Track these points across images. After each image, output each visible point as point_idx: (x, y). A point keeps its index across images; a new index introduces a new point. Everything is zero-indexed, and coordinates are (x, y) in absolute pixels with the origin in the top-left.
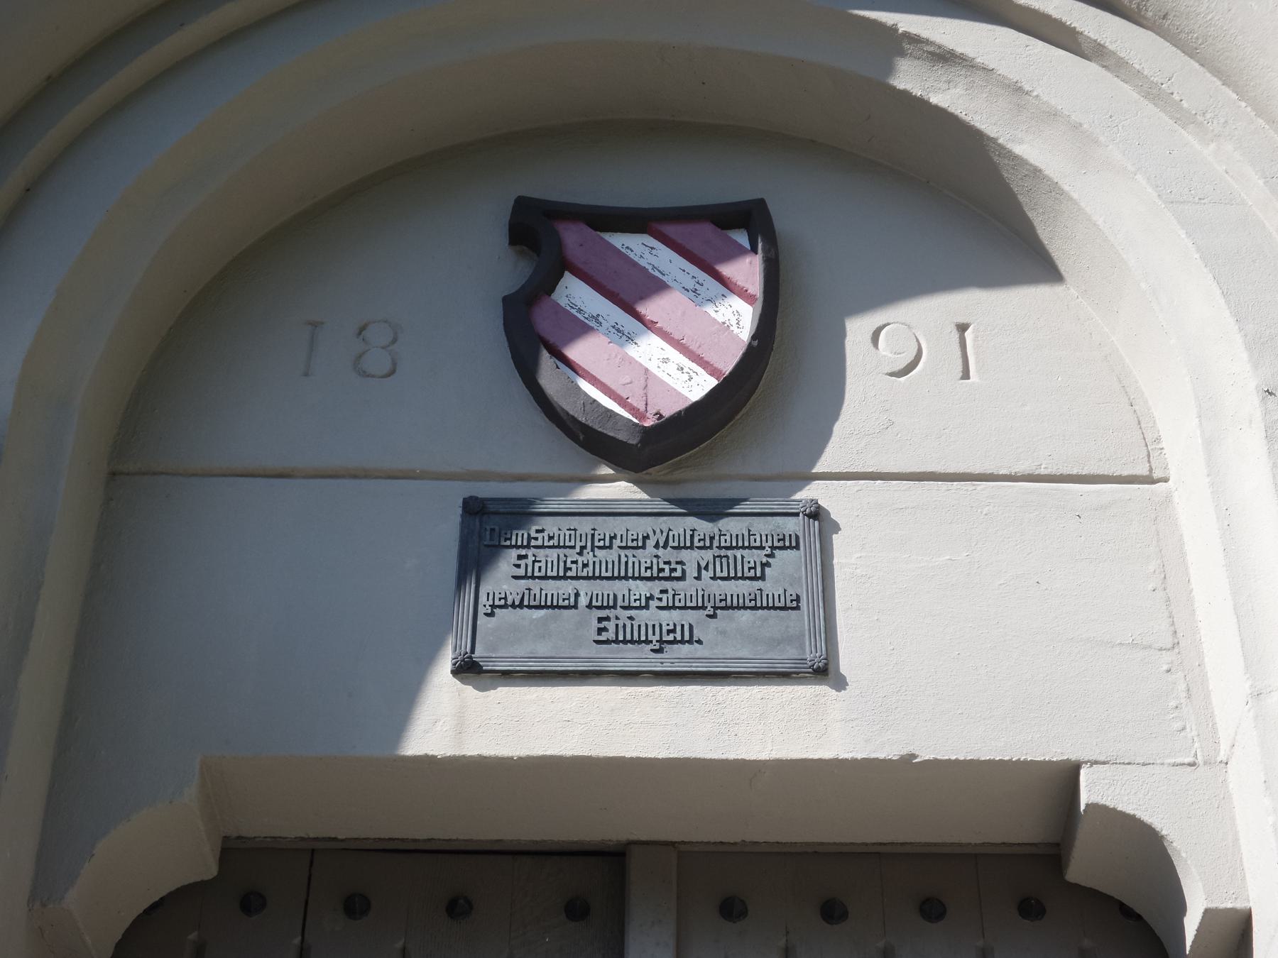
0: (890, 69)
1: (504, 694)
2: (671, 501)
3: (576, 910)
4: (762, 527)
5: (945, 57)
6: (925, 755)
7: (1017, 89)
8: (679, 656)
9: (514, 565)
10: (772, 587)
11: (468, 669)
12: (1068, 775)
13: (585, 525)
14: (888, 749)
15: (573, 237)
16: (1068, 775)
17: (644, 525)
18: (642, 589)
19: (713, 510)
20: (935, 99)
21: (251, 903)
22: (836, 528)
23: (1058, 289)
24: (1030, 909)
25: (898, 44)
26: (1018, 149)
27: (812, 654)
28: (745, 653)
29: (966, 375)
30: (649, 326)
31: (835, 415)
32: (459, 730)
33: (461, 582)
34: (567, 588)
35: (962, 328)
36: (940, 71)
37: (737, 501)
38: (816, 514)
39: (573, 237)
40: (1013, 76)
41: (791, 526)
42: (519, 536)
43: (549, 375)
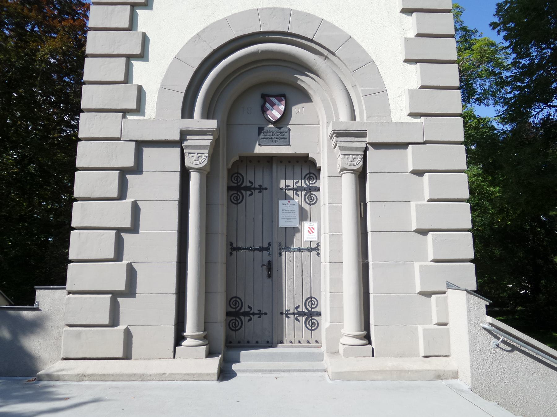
0: (297, 81)
1: (263, 147)
2: (276, 128)
3: (268, 162)
4: (284, 130)
5: (303, 81)
6: (297, 152)
7: (309, 86)
8: (277, 144)
9: (258, 318)
10: (285, 137)
11: (259, 145)
12: (308, 154)
13: (269, 130)
14: (294, 152)
15: (267, 98)
16: (308, 154)
17: (273, 130)
18: (274, 137)
19: (280, 128)
20: (301, 85)
21: (242, 161)
22: (291, 130)
23: (312, 103)
24: (306, 162)
25: (298, 79)
26: (309, 91)
27: (288, 143)
28: (282, 143)
29: (303, 113)
30: (274, 109)
31: (291, 118)
32: (259, 150)
33: (258, 136)
34: (267, 137)
35: (303, 108)
36: (302, 82)
37: (282, 128)
38: (289, 129)
39: (267, 98)
40: (309, 84)
41: (287, 130)
42: (263, 131)
43: (265, 115)
